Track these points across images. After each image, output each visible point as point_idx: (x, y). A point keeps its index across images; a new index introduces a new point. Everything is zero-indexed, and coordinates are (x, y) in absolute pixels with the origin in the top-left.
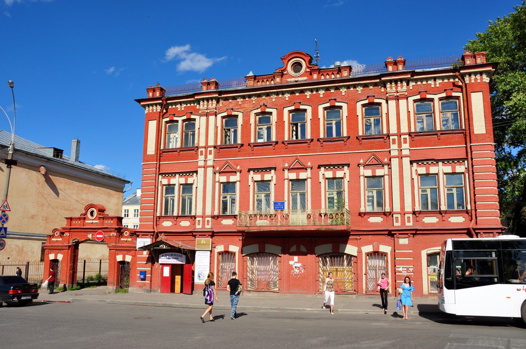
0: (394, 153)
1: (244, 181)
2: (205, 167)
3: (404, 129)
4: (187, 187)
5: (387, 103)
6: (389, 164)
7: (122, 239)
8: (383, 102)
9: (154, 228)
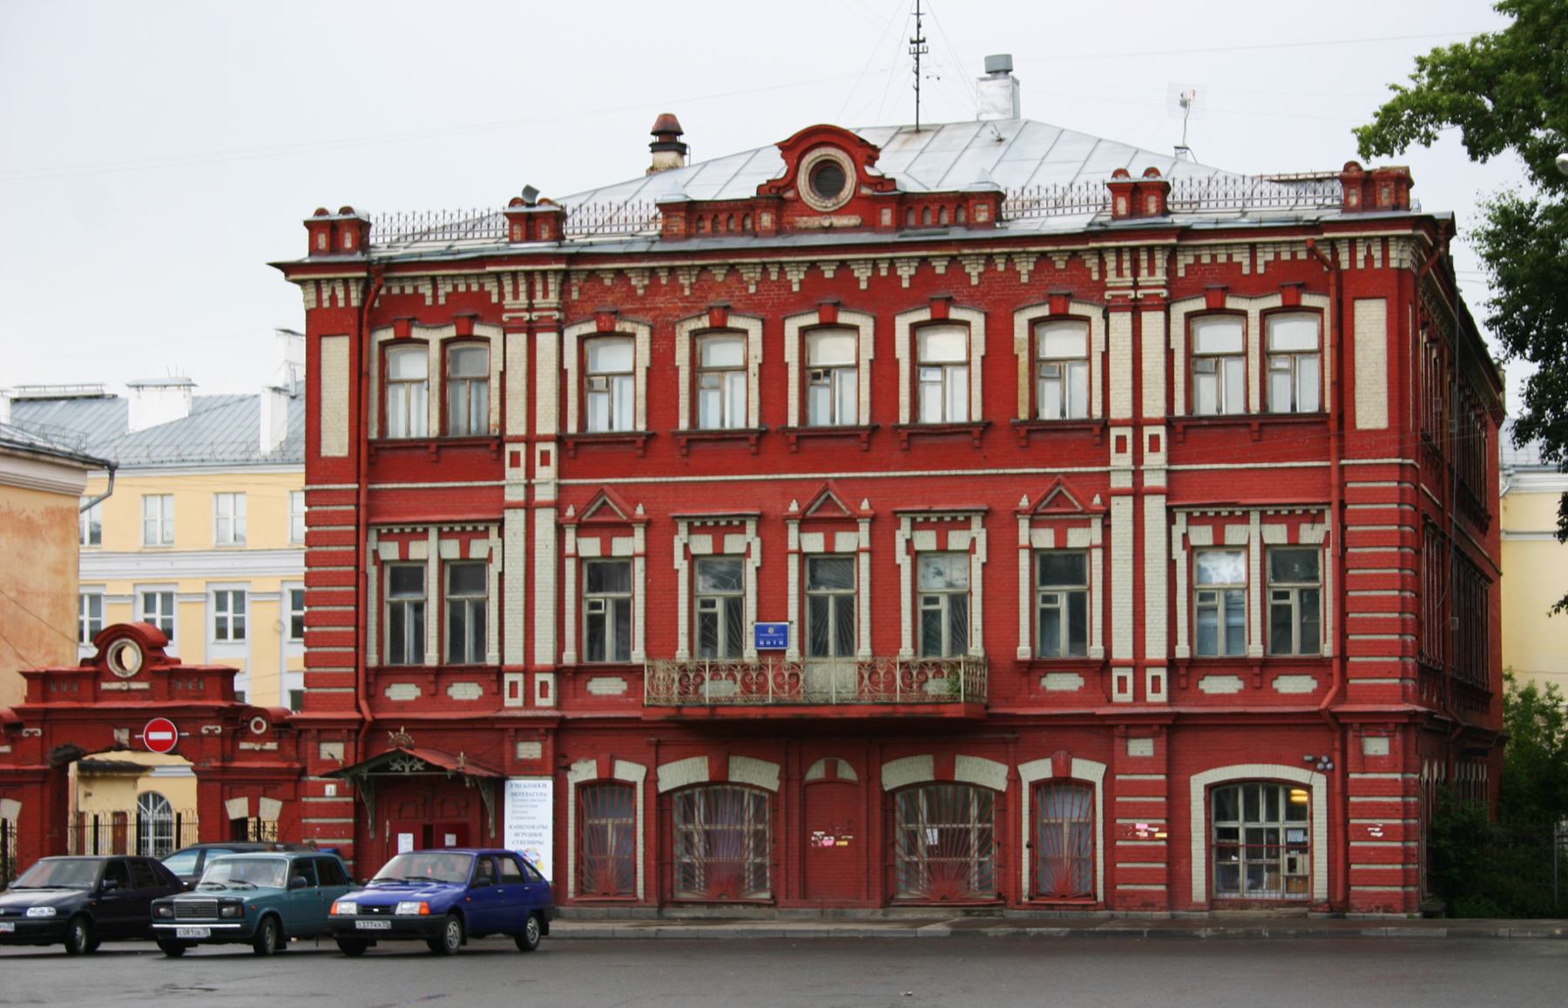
0: (1121, 481)
1: (658, 555)
2: (1138, 494)
3: (1154, 406)
4: (466, 574)
5: (1106, 318)
6: (1107, 515)
7: (244, 746)
8: (1095, 314)
9: (359, 709)
